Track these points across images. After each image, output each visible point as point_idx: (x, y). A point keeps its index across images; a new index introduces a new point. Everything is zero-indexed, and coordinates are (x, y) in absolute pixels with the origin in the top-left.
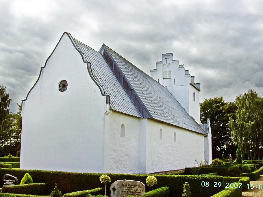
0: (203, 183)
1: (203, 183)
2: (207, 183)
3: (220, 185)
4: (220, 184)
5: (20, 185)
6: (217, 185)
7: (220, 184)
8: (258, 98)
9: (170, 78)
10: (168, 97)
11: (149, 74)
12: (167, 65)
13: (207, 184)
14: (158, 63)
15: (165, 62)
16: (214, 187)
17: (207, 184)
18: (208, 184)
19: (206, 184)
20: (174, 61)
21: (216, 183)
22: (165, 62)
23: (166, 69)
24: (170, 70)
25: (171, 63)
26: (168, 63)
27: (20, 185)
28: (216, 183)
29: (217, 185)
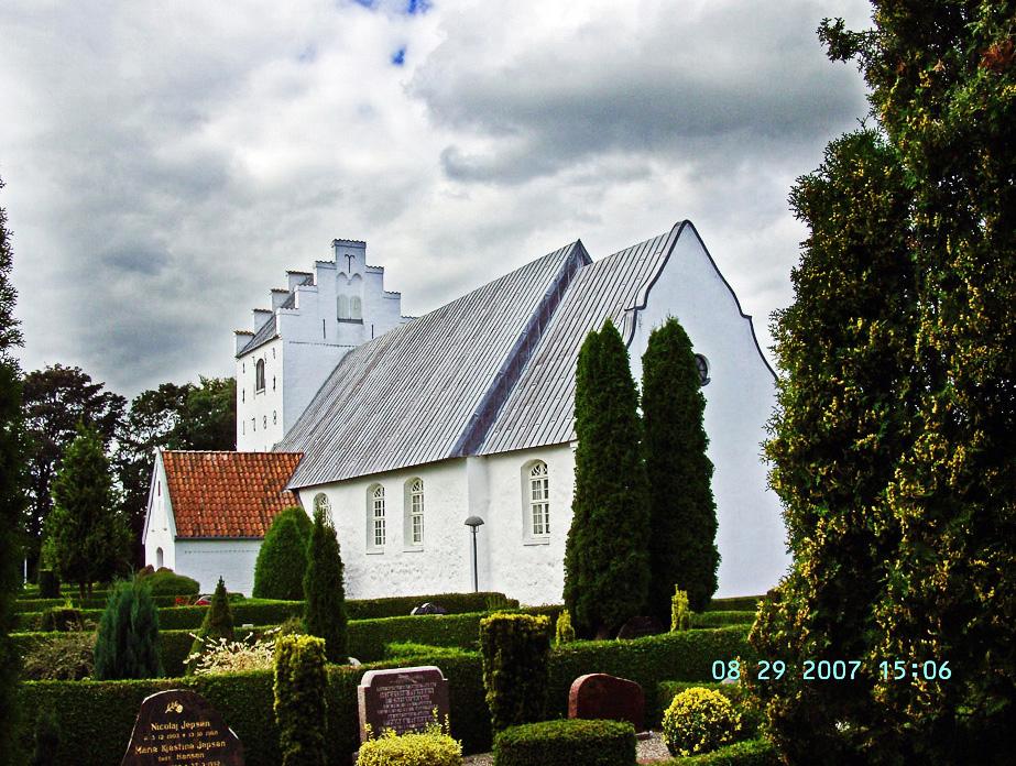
0: (719, 666)
1: (719, 666)
2: (734, 665)
3: (782, 672)
4: (779, 667)
5: (672, 633)
6: (770, 673)
7: (779, 667)
8: (245, 599)
9: (361, 322)
10: (161, 587)
11: (258, 354)
12: (349, 276)
13: (732, 669)
14: (322, 265)
15: (342, 267)
16: (805, 677)
17: (732, 669)
18: (735, 669)
19: (727, 669)
20: (371, 270)
21: (764, 666)
22: (342, 267)
23: (351, 291)
24: (357, 294)
25: (362, 274)
26: (353, 272)
27: (672, 633)
28: (764, 666)
29: (770, 673)
